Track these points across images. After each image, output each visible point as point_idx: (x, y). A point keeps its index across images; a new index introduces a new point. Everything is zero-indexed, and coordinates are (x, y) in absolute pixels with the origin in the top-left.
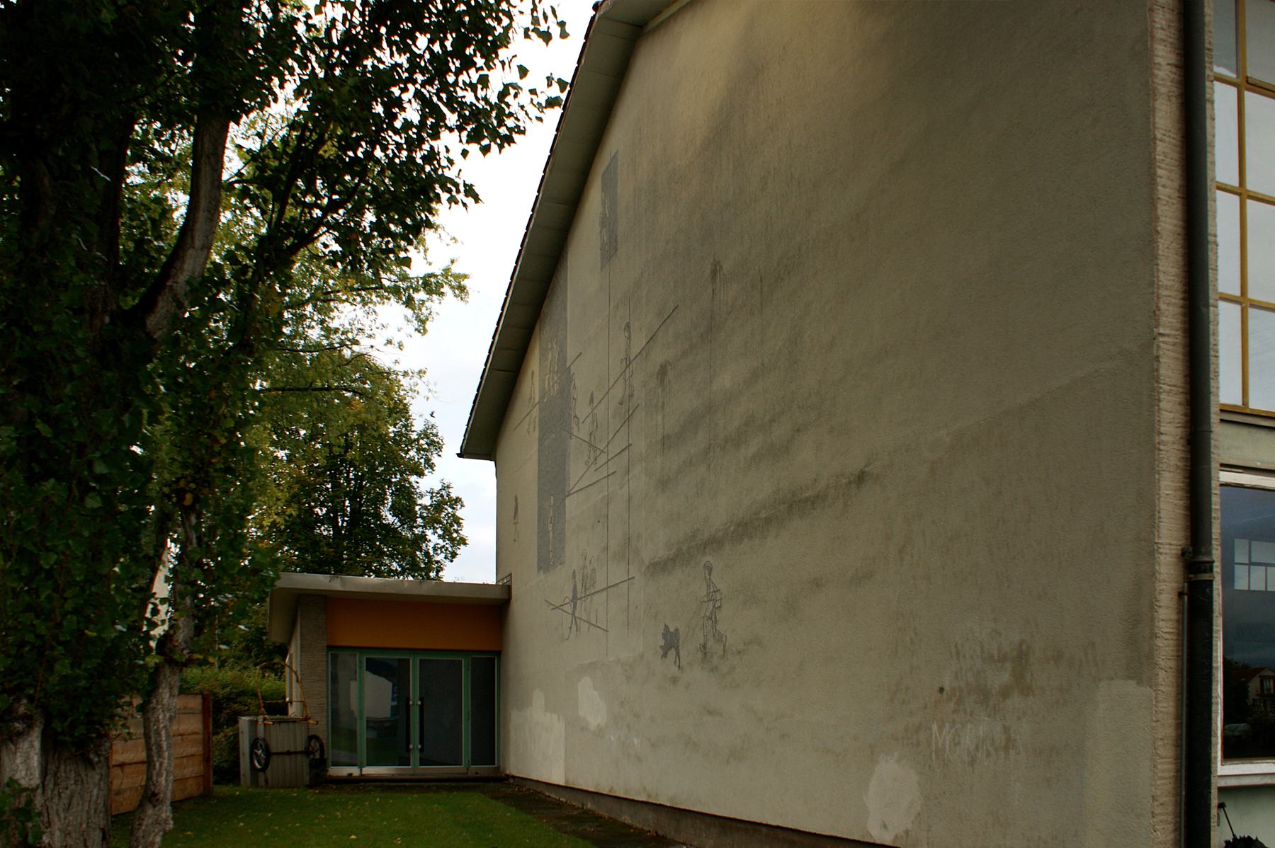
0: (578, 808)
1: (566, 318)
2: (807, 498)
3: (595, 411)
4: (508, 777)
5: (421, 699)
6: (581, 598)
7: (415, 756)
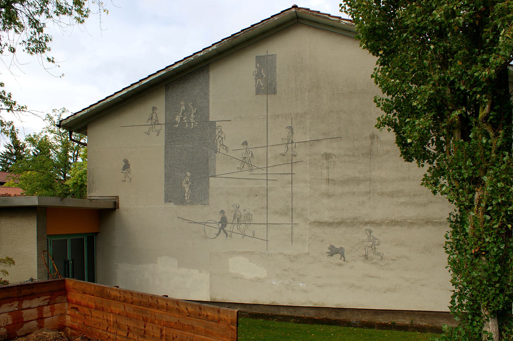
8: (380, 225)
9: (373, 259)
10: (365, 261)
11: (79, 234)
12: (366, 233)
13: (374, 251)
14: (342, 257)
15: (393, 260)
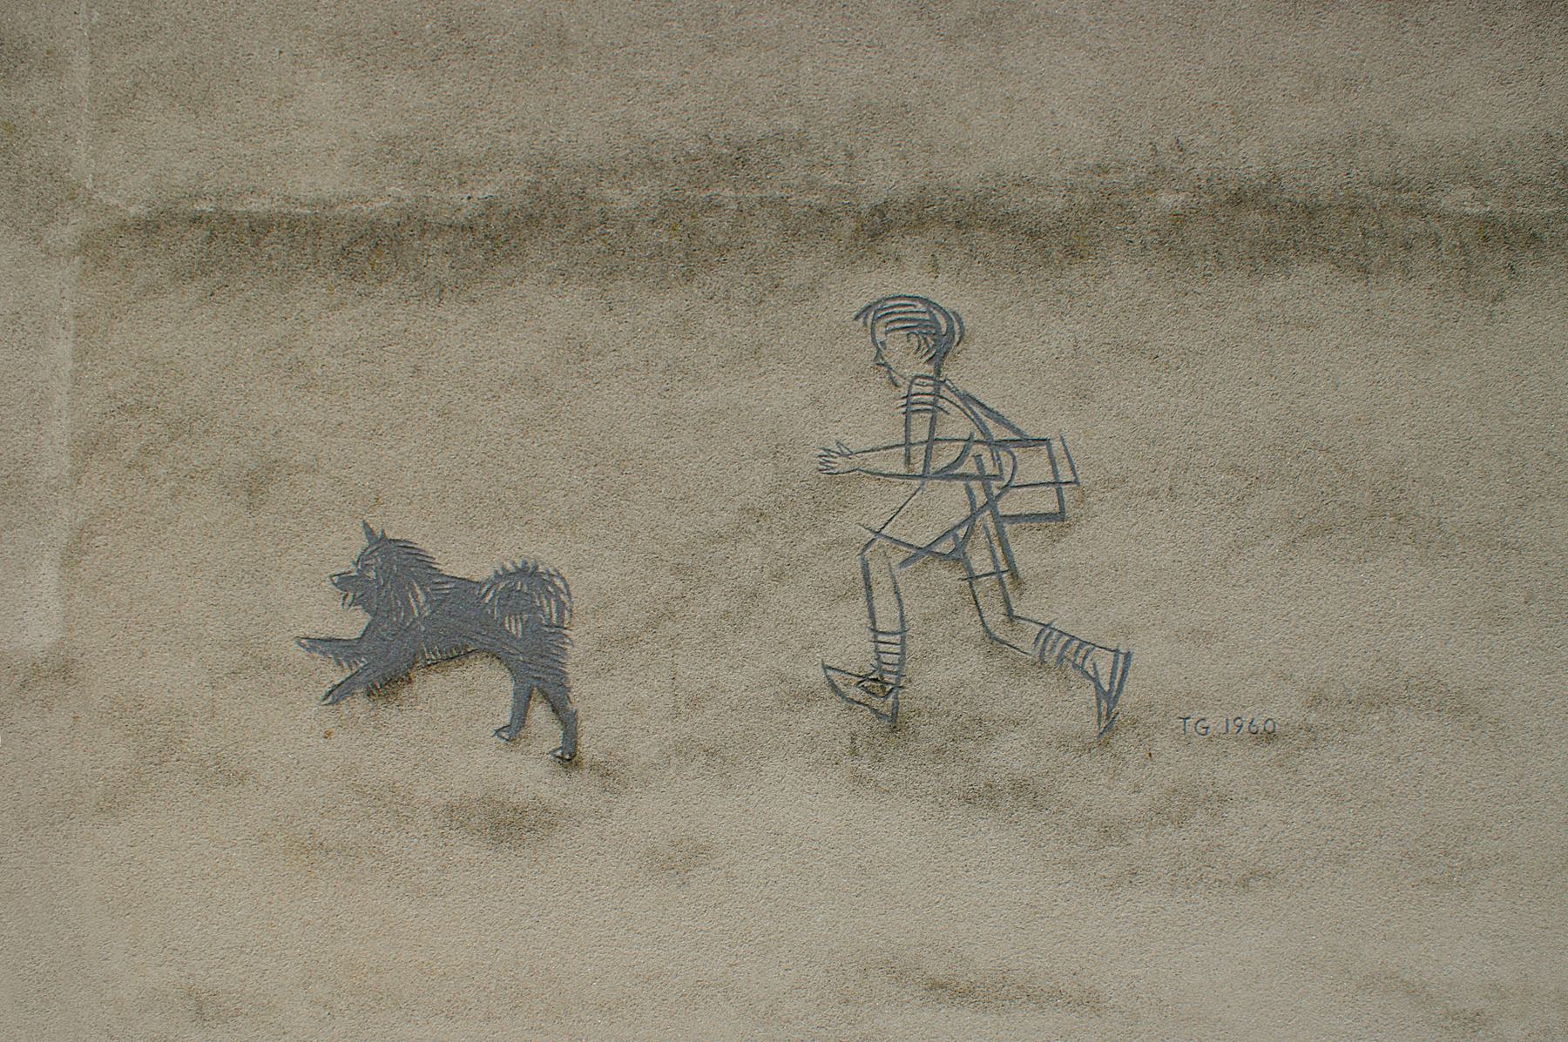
8: (1072, 253)
9: (980, 727)
12: (880, 363)
13: (995, 616)
14: (540, 713)
15: (1270, 736)
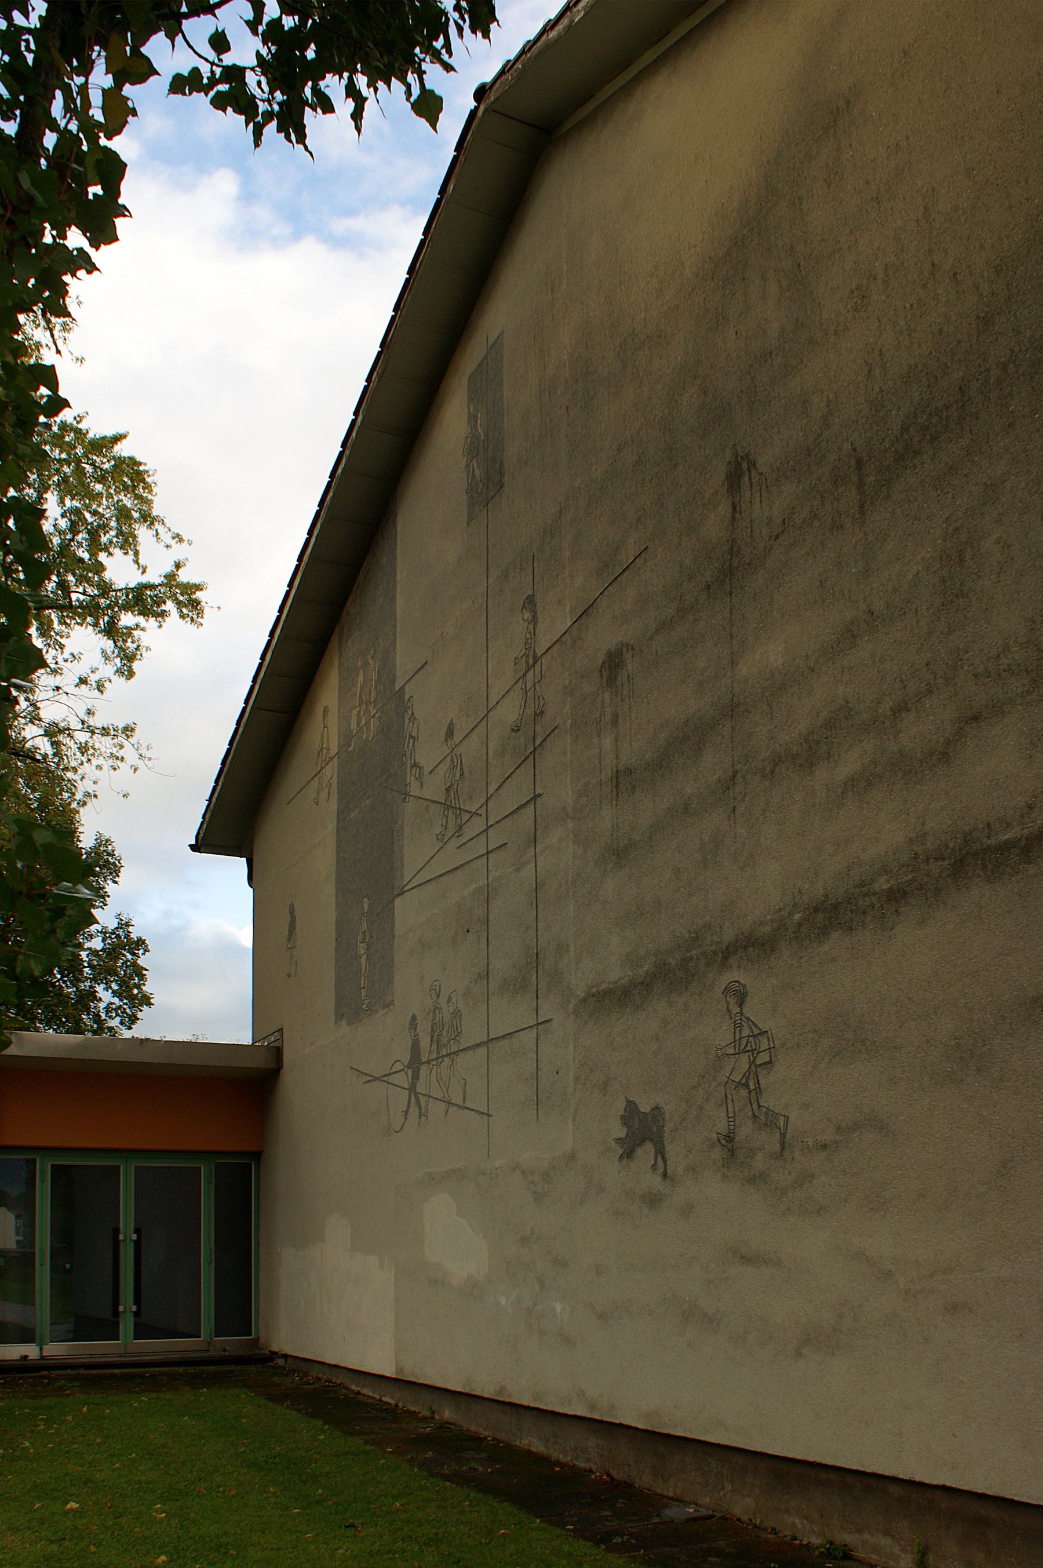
0: (425, 1419)
1: (394, 614)
2: (1006, 842)
3: (458, 751)
4: (274, 1355)
5: (137, 1231)
6: (428, 1062)
7: (127, 1326)
10: (725, 1170)
11: (170, 1151)
